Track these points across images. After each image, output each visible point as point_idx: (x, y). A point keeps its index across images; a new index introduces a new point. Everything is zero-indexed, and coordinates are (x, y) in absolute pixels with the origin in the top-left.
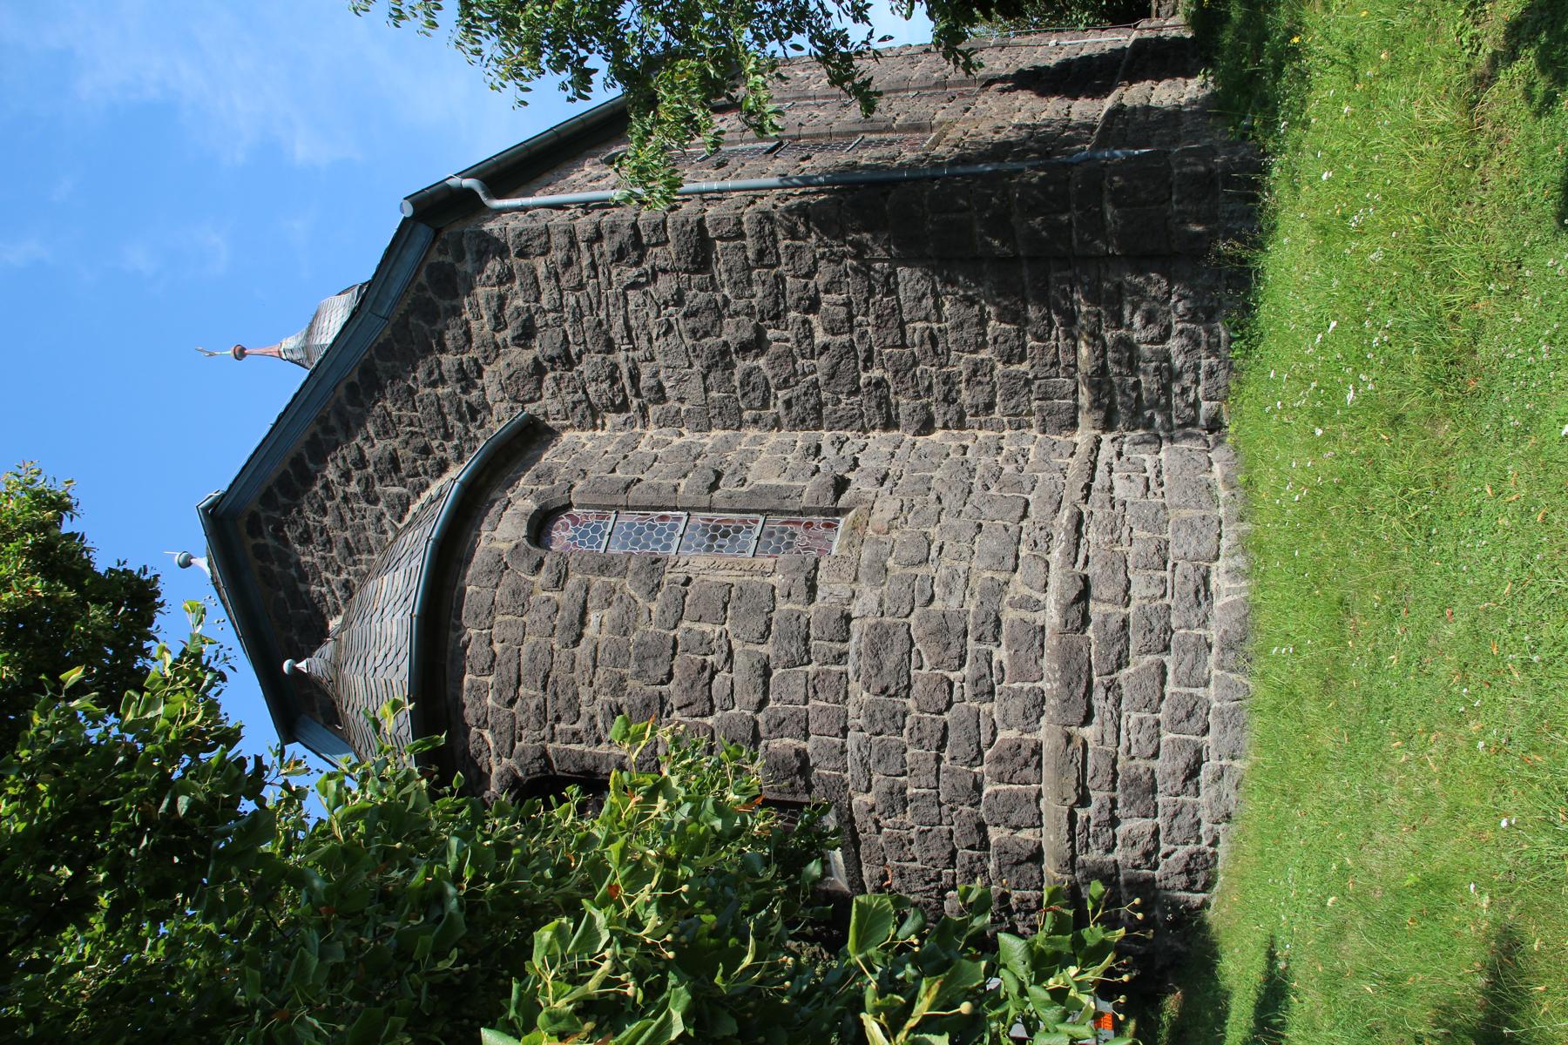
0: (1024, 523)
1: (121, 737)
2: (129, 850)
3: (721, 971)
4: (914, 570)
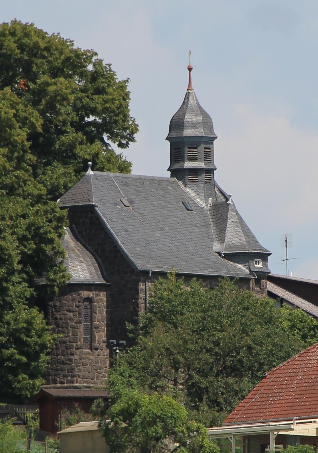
0: (90, 379)
1: (59, 140)
2: (224, 371)
3: (60, 432)
4: (81, 363)
